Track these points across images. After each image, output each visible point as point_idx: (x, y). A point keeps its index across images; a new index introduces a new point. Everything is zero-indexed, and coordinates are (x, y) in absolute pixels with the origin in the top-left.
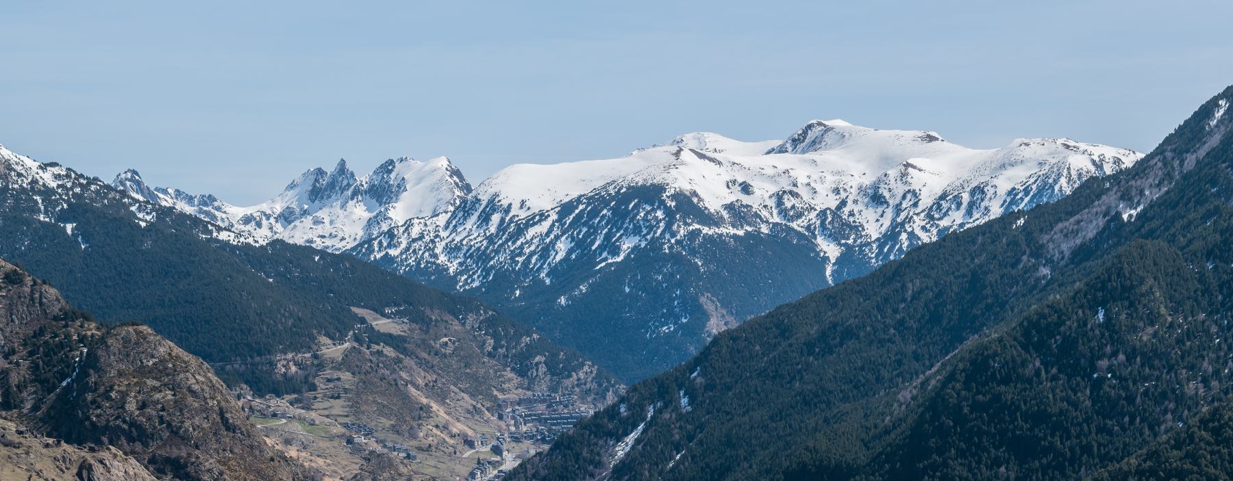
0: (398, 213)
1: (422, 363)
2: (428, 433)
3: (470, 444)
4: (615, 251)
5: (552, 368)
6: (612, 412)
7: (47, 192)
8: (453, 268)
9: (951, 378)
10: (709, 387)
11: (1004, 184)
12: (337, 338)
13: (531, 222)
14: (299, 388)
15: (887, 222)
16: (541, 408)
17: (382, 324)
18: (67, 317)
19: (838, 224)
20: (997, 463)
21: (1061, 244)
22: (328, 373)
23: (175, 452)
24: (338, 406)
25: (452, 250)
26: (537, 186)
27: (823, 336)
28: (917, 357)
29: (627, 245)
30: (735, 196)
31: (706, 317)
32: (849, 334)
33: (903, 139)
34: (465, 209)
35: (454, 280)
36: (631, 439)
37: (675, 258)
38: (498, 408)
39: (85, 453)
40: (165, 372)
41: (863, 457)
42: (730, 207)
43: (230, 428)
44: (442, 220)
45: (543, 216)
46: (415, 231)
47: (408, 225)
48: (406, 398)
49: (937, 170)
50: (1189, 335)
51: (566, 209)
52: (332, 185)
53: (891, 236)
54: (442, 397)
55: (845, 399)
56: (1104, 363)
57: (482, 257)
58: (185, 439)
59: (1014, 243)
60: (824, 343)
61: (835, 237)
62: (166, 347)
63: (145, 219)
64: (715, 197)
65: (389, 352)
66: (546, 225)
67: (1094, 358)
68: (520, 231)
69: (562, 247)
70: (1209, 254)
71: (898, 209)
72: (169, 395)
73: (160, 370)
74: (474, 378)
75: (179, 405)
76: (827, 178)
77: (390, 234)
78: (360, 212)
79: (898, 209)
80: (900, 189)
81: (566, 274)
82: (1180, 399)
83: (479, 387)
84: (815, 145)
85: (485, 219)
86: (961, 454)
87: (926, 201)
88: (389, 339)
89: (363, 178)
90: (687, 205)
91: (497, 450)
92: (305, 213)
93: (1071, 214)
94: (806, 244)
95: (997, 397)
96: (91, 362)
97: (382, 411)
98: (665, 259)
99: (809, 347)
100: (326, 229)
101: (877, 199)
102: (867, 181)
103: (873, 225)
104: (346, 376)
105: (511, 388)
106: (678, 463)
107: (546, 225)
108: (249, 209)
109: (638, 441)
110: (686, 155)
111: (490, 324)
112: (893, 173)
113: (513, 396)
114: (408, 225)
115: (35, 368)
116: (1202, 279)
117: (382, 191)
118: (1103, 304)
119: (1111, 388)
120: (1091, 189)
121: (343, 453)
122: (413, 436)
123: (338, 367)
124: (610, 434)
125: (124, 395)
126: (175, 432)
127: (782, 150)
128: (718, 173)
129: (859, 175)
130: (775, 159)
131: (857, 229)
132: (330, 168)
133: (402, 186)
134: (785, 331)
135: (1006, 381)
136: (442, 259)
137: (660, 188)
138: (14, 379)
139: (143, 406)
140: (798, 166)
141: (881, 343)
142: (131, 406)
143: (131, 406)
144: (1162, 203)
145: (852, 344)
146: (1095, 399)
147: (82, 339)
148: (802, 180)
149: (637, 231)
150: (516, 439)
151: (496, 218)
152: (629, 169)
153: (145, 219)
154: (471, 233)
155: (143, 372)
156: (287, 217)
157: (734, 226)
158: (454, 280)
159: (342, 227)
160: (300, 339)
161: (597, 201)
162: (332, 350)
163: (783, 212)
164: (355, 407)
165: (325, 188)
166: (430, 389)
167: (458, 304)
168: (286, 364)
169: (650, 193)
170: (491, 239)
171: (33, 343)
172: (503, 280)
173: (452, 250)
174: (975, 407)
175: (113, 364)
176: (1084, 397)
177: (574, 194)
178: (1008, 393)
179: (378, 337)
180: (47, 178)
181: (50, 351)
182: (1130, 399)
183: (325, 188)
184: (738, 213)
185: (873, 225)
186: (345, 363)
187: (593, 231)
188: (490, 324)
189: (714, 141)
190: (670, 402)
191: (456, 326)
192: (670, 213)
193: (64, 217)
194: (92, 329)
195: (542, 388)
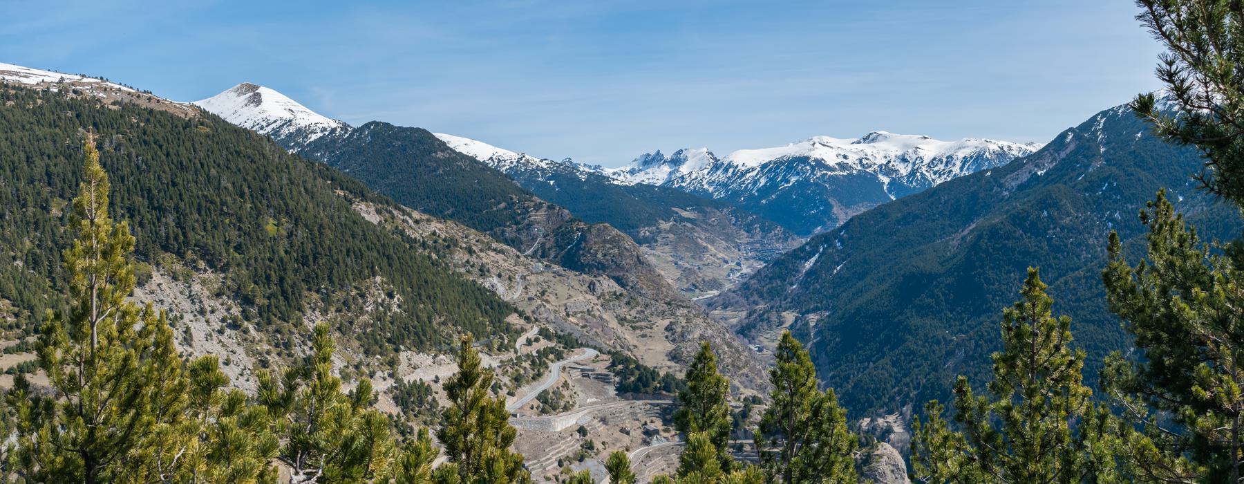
0: (684, 169)
1: (704, 229)
2: (707, 258)
3: (726, 262)
4: (788, 182)
5: (763, 229)
6: (802, 249)
7: (543, 170)
8: (711, 190)
9: (980, 237)
10: (851, 238)
11: (961, 154)
12: (667, 220)
13: (747, 171)
14: (650, 241)
15: (909, 169)
16: (758, 246)
17: (685, 214)
18: (572, 221)
19: (887, 169)
20: (1009, 272)
21: (1012, 182)
22: (663, 235)
23: (618, 274)
24: (667, 248)
25: (710, 183)
26: (750, 158)
27: (904, 218)
28: (951, 226)
29: (793, 179)
30: (841, 160)
31: (832, 207)
32: (916, 217)
33: (914, 139)
34: (717, 166)
35: (712, 194)
36: (813, 260)
37: (817, 184)
38: (738, 246)
39: (592, 278)
40: (615, 242)
41: (942, 270)
42: (839, 164)
43: (640, 262)
44: (706, 171)
45: (753, 169)
46: (693, 176)
47: (690, 174)
48: (697, 243)
49: (930, 150)
50: (1085, 220)
51: (764, 166)
52: (653, 159)
53: (913, 174)
54: (713, 242)
55: (920, 243)
56: (1051, 232)
57: (725, 185)
58: (622, 268)
59: (988, 182)
60: (906, 220)
61: (887, 174)
62: (615, 232)
63: (583, 178)
64: (832, 160)
65: (689, 225)
66: (755, 173)
67: (1046, 230)
68: (743, 175)
69: (763, 181)
70: (1086, 190)
71: (914, 164)
72: (616, 251)
73: (612, 241)
74: (727, 234)
75: (621, 255)
76: (878, 153)
77: (682, 178)
78: (666, 169)
79: (914, 164)
80: (914, 157)
81: (764, 191)
82: (1087, 246)
83: (729, 238)
84: (873, 140)
85: (726, 170)
86: (992, 268)
87: (927, 161)
88: (689, 220)
89: (668, 156)
90: (820, 164)
91: (738, 264)
92: (640, 170)
93: (1012, 172)
94: (874, 177)
95: (1005, 245)
96: (583, 238)
97: (687, 250)
98: (812, 185)
99: (898, 222)
100: (651, 176)
101: (904, 160)
102: (899, 153)
103: (904, 170)
104: (671, 236)
105: (744, 238)
106: (839, 272)
107: (755, 173)
108: (620, 171)
109: (816, 261)
110: (817, 145)
111: (734, 212)
112: (910, 151)
113: (744, 241)
114: (690, 174)
115: (557, 241)
116: (1085, 199)
117: (677, 161)
118: (1046, 208)
119: (1055, 241)
120: (1017, 164)
121: (673, 267)
122: (701, 259)
123: (668, 232)
124: (802, 258)
125: (597, 251)
126: (618, 266)
127: (859, 142)
128: (832, 150)
129: (894, 151)
130: (855, 146)
131: (896, 171)
132: (653, 153)
133: (686, 159)
134: (885, 216)
135: (1008, 238)
136: (706, 186)
137: (808, 158)
138: (547, 246)
139: (605, 255)
140: (868, 149)
141: (933, 221)
142: (600, 256)
143: (600, 256)
144: (1055, 169)
145: (918, 221)
146: (1050, 246)
147: (578, 230)
148: (869, 153)
149: (798, 174)
150: (747, 259)
151: (731, 170)
152: (791, 150)
153: (583, 178)
154: (720, 176)
155: (605, 241)
156: (632, 172)
157: (994, 233)
158: (712, 194)
159: (658, 176)
160: (651, 221)
161: (778, 163)
162: (665, 226)
163: (862, 165)
164: (675, 248)
165: (650, 161)
166: (708, 240)
167: (718, 204)
168: (644, 232)
169: (804, 160)
170: (729, 178)
171: (556, 232)
172: (736, 194)
173: (710, 183)
174: (994, 249)
175: (592, 238)
176: (1045, 244)
177: (767, 160)
178: (1010, 244)
179: (684, 219)
180: (543, 165)
181: (564, 234)
182: (1066, 246)
183: (650, 161)
184: (842, 166)
185: (904, 170)
186: (670, 231)
187: (777, 174)
188: (734, 212)
189: (826, 139)
190: (831, 245)
191: (718, 213)
192: (812, 167)
193: (550, 178)
194: (582, 225)
195: (758, 237)
